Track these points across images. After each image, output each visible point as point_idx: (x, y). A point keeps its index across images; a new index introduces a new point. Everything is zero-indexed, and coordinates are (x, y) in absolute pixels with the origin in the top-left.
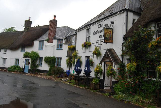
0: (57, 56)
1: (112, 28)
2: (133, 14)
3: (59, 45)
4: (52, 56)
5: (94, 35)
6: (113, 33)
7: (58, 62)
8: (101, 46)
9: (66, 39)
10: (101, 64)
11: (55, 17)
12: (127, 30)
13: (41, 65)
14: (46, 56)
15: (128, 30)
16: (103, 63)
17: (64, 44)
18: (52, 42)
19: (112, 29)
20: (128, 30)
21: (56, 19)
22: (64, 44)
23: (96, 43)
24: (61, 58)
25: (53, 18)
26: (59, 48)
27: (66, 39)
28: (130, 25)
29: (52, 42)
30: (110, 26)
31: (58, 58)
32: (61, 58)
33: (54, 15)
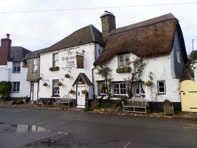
0: (13, 80)
1: (83, 55)
2: (100, 45)
3: (16, 68)
4: (7, 81)
5: (76, 53)
6: (83, 59)
7: (15, 87)
8: (71, 70)
9: (24, 62)
10: (74, 86)
11: (8, 35)
12: (95, 58)
13: (170, 30)
14: (93, 63)
15: (97, 58)
16: (75, 86)
17: (22, 67)
18: (6, 64)
19: (83, 56)
20: (97, 59)
21: (10, 38)
22: (22, 67)
23: (67, 68)
24: (19, 83)
25: (6, 37)
26: (16, 71)
27: (24, 62)
28: (98, 55)
29: (6, 64)
30: (81, 54)
31: (15, 83)
32: (19, 83)
33: (7, 34)
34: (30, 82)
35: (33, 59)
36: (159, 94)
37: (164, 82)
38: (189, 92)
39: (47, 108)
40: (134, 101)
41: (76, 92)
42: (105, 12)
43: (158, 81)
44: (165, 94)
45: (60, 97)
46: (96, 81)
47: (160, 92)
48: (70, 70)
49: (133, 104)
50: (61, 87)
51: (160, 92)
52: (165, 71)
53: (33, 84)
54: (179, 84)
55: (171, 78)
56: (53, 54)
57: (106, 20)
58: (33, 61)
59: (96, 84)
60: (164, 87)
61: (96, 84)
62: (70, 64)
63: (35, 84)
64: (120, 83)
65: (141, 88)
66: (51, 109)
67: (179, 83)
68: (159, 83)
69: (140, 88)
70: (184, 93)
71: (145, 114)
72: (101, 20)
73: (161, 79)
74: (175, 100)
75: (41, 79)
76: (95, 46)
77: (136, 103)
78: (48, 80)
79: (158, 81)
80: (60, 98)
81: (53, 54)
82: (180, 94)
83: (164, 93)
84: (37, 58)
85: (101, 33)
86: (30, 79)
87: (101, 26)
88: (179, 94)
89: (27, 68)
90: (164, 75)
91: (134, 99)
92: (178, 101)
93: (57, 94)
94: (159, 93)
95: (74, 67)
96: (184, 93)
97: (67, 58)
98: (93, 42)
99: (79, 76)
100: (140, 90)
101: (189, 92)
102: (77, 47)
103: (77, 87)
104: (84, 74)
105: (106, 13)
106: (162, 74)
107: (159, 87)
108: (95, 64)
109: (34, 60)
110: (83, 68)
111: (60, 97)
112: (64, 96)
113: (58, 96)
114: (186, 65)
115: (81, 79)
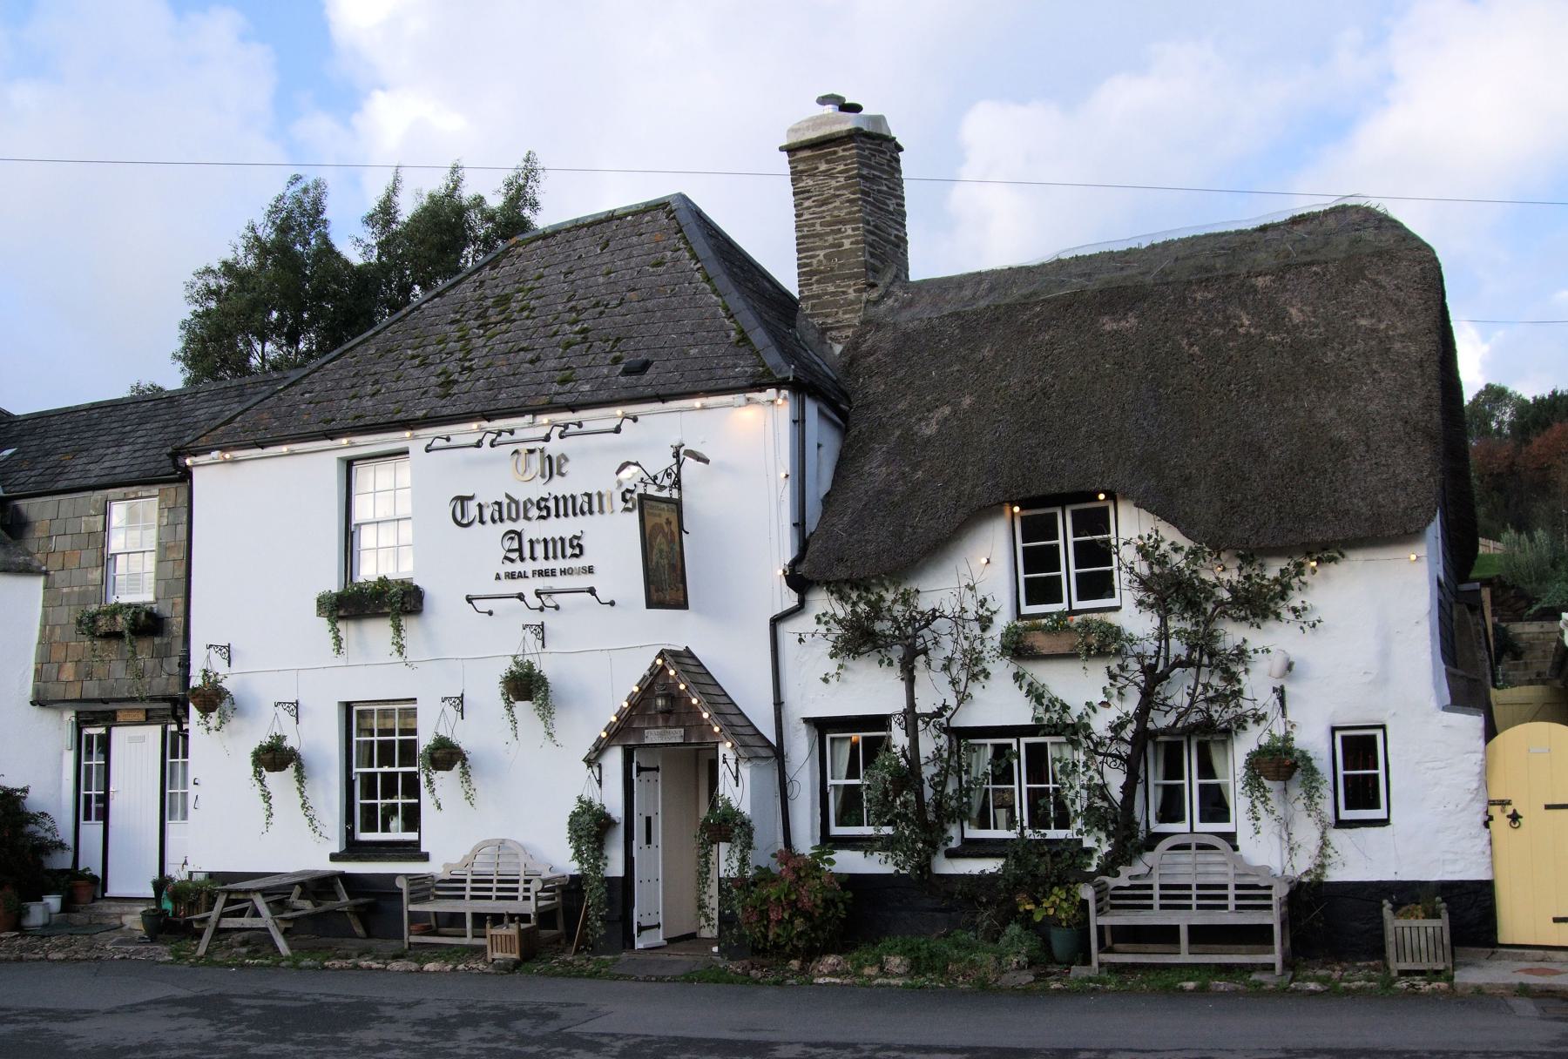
1: (675, 495)
8: (548, 618)
12: (799, 525)
23: (521, 597)
34: (69, 716)
35: (98, 495)
36: (1341, 824)
37: (1379, 734)
38: (1548, 807)
39: (414, 966)
40: (1203, 880)
41: (69, 841)
42: (824, 100)
43: (1334, 730)
44: (1384, 822)
45: (425, 857)
46: (807, 720)
47: (1202, 820)
48: (536, 618)
49: (1194, 892)
50: (445, 782)
51: (1348, 807)
52: (1385, 655)
53: (105, 743)
54: (1485, 752)
55: (1432, 704)
56: (341, 459)
57: (839, 173)
58: (106, 513)
59: (800, 747)
60: (1381, 771)
61: (800, 747)
62: (541, 564)
63: (119, 736)
64: (1024, 740)
65: (1196, 782)
66: (395, 966)
67: (1481, 742)
68: (1344, 738)
69: (1192, 783)
70: (1515, 817)
71: (1270, 967)
72: (786, 169)
73: (1355, 715)
74: (1449, 868)
75: (213, 699)
76: (799, 422)
77: (1175, 895)
78: (461, 699)
79: (1334, 730)
80: (434, 867)
81: (341, 459)
82: (1486, 825)
83: (1379, 814)
84: (155, 490)
85: (786, 294)
86: (74, 693)
87: (791, 221)
88: (1480, 818)
89: (39, 583)
90: (1382, 680)
91: (1155, 866)
92: (1472, 871)
93: (397, 833)
94: (1346, 815)
95: (592, 591)
96: (1515, 817)
97: (508, 509)
98: (779, 386)
99: (656, 673)
100: (1192, 801)
101: (1548, 807)
102: (619, 411)
103: (768, 758)
104: (688, 653)
105: (848, 122)
106: (1371, 677)
107: (1341, 772)
108: (799, 581)
109: (119, 512)
110: (683, 604)
111: (425, 857)
112: (467, 850)
113: (412, 851)
114: (1465, 587)
115: (674, 697)
